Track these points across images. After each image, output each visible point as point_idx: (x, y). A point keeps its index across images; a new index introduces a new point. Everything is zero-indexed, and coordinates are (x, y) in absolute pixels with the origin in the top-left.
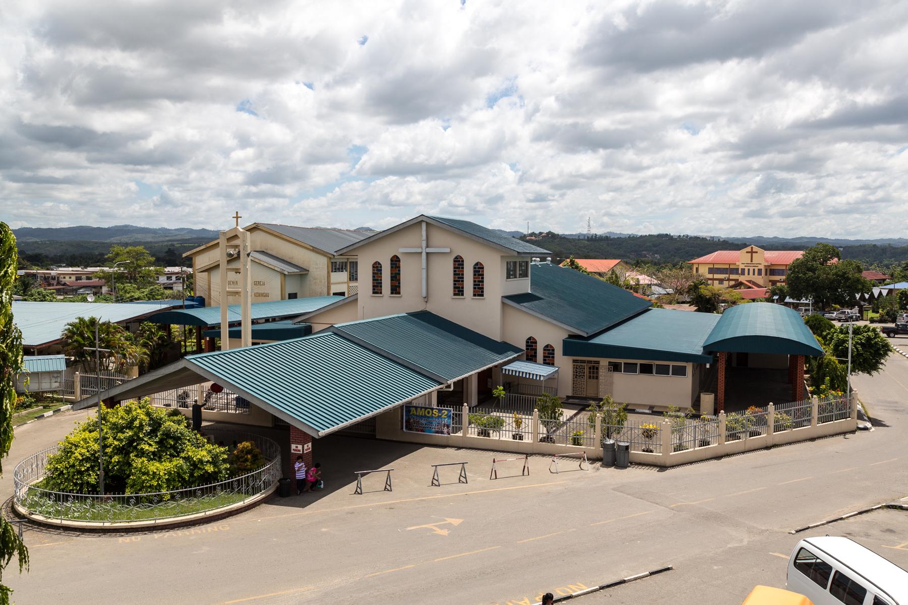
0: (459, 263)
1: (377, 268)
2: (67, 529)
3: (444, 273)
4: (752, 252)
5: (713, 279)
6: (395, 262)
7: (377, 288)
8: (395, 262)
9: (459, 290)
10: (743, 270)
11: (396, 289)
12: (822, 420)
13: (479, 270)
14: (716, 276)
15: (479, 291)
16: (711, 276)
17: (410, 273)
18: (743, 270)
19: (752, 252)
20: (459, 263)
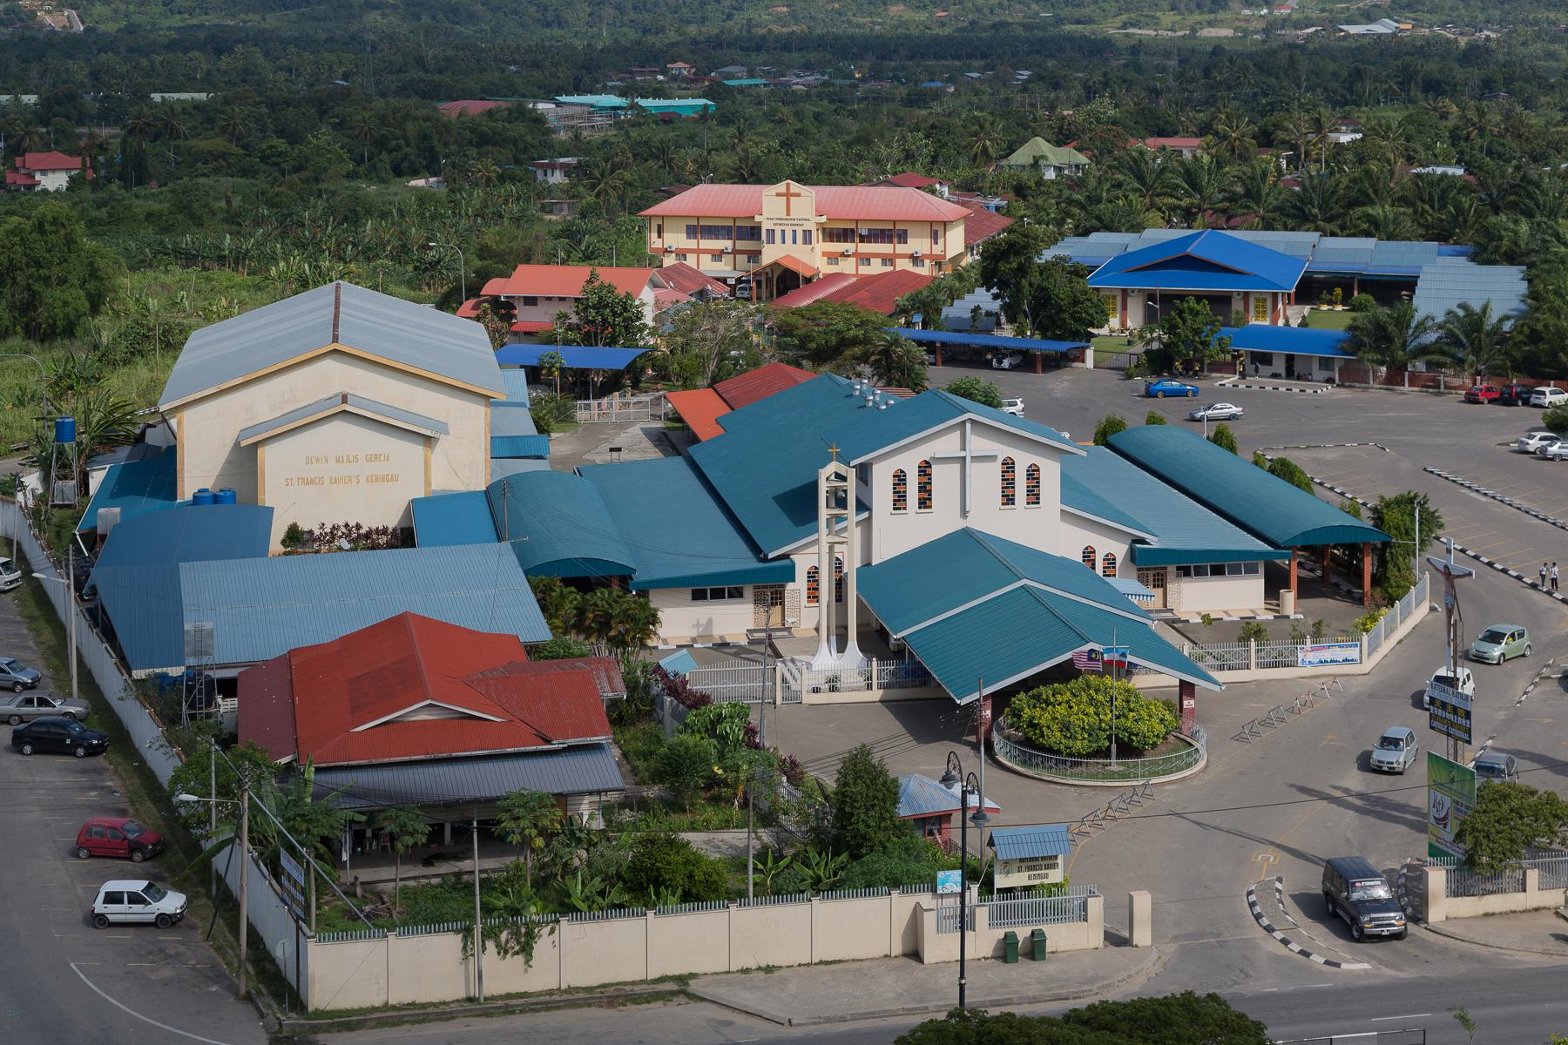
0: (1009, 466)
1: (900, 478)
2: (854, 1018)
3: (986, 480)
4: (788, 195)
5: (698, 251)
6: (925, 469)
7: (899, 500)
8: (925, 469)
9: (1009, 500)
10: (771, 233)
11: (924, 503)
12: (1260, 666)
13: (1033, 474)
14: (708, 244)
15: (1034, 496)
16: (692, 244)
17: (944, 479)
18: (771, 233)
19: (788, 195)
20: (1009, 466)
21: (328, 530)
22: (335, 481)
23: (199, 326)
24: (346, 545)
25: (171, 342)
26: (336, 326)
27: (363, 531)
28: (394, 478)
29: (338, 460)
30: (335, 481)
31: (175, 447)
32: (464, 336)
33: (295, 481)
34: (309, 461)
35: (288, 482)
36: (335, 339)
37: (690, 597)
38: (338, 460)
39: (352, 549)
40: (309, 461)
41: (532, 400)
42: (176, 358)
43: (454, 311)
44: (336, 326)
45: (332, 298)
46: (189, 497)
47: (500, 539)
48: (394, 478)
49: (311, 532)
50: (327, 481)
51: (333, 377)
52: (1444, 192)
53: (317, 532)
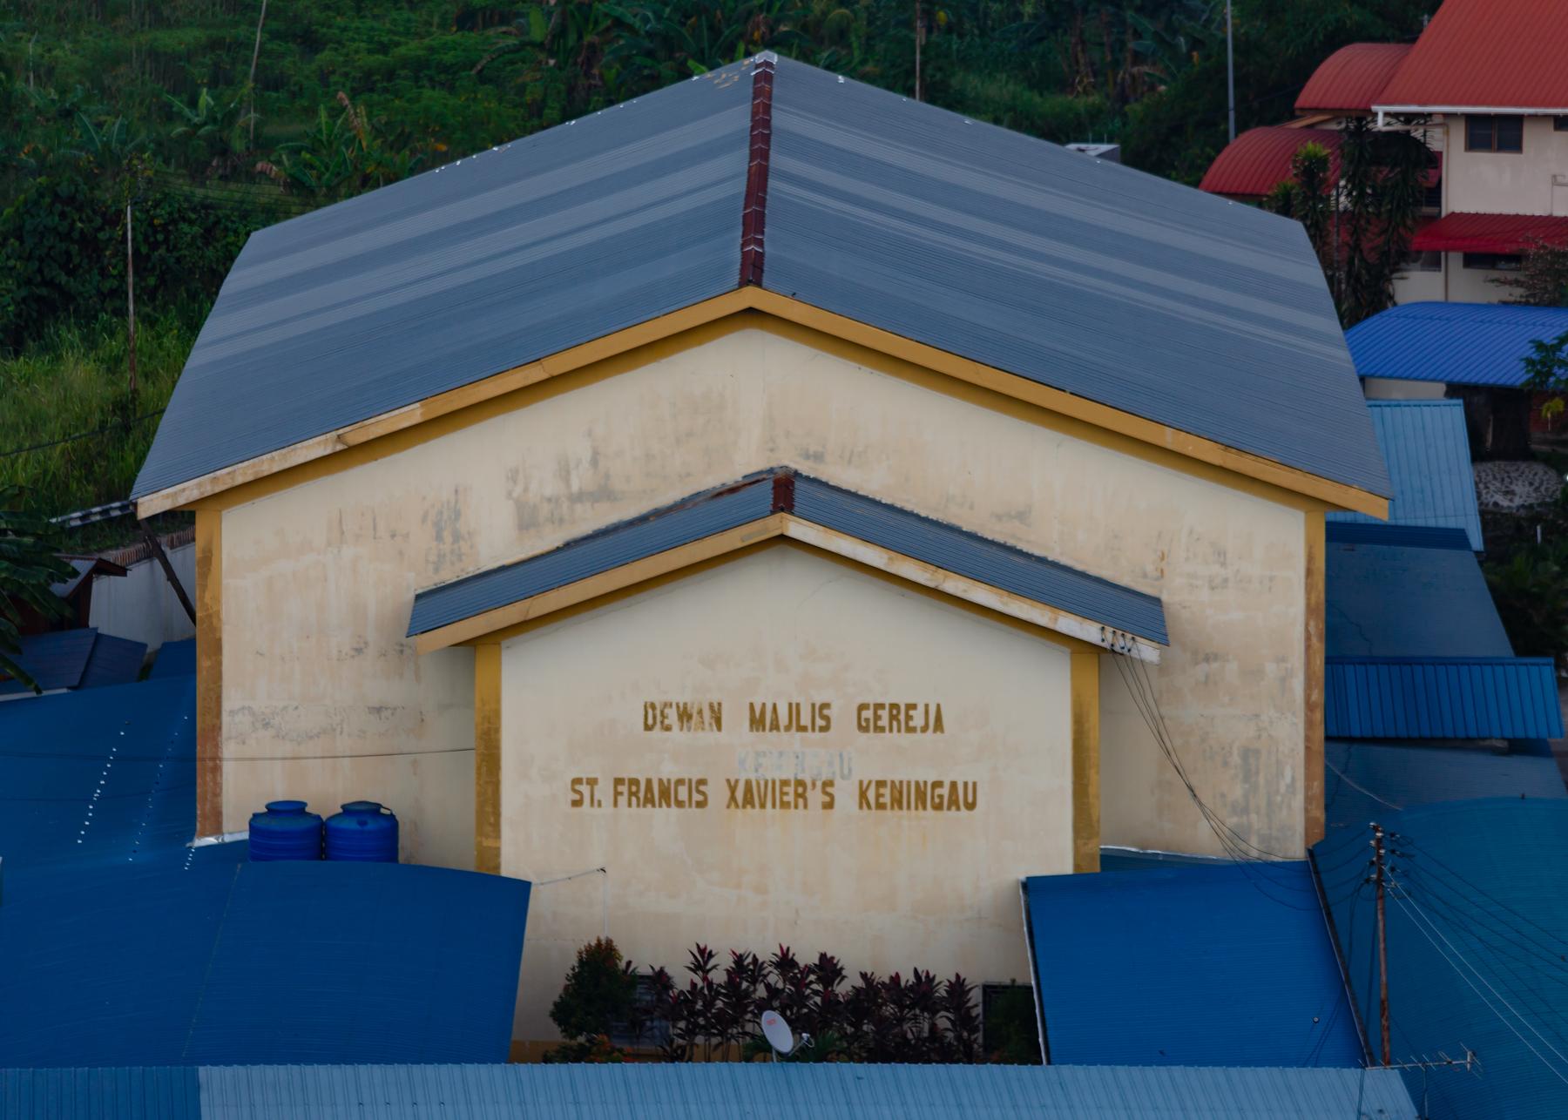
9: (975, 784)
21: (719, 977)
22: (747, 796)
23: (272, 215)
24: (780, 1034)
25: (185, 278)
26: (754, 223)
27: (842, 989)
28: (960, 798)
29: (757, 722)
30: (747, 796)
31: (190, 645)
32: (1250, 264)
33: (604, 790)
34: (654, 718)
35: (581, 791)
36: (753, 271)
37: (538, 904)
38: (757, 722)
39: (800, 1055)
40: (654, 718)
41: (1490, 518)
42: (193, 327)
43: (1193, 175)
44: (754, 223)
45: (739, 119)
46: (236, 830)
47: (1363, 1055)
48: (960, 798)
49: (660, 979)
50: (717, 793)
51: (754, 399)
52: (850, 462)
53: (682, 979)
